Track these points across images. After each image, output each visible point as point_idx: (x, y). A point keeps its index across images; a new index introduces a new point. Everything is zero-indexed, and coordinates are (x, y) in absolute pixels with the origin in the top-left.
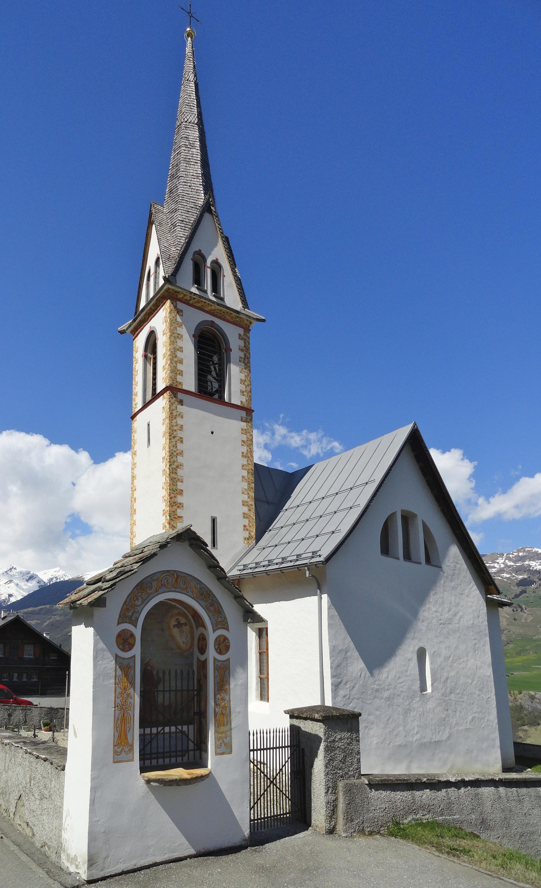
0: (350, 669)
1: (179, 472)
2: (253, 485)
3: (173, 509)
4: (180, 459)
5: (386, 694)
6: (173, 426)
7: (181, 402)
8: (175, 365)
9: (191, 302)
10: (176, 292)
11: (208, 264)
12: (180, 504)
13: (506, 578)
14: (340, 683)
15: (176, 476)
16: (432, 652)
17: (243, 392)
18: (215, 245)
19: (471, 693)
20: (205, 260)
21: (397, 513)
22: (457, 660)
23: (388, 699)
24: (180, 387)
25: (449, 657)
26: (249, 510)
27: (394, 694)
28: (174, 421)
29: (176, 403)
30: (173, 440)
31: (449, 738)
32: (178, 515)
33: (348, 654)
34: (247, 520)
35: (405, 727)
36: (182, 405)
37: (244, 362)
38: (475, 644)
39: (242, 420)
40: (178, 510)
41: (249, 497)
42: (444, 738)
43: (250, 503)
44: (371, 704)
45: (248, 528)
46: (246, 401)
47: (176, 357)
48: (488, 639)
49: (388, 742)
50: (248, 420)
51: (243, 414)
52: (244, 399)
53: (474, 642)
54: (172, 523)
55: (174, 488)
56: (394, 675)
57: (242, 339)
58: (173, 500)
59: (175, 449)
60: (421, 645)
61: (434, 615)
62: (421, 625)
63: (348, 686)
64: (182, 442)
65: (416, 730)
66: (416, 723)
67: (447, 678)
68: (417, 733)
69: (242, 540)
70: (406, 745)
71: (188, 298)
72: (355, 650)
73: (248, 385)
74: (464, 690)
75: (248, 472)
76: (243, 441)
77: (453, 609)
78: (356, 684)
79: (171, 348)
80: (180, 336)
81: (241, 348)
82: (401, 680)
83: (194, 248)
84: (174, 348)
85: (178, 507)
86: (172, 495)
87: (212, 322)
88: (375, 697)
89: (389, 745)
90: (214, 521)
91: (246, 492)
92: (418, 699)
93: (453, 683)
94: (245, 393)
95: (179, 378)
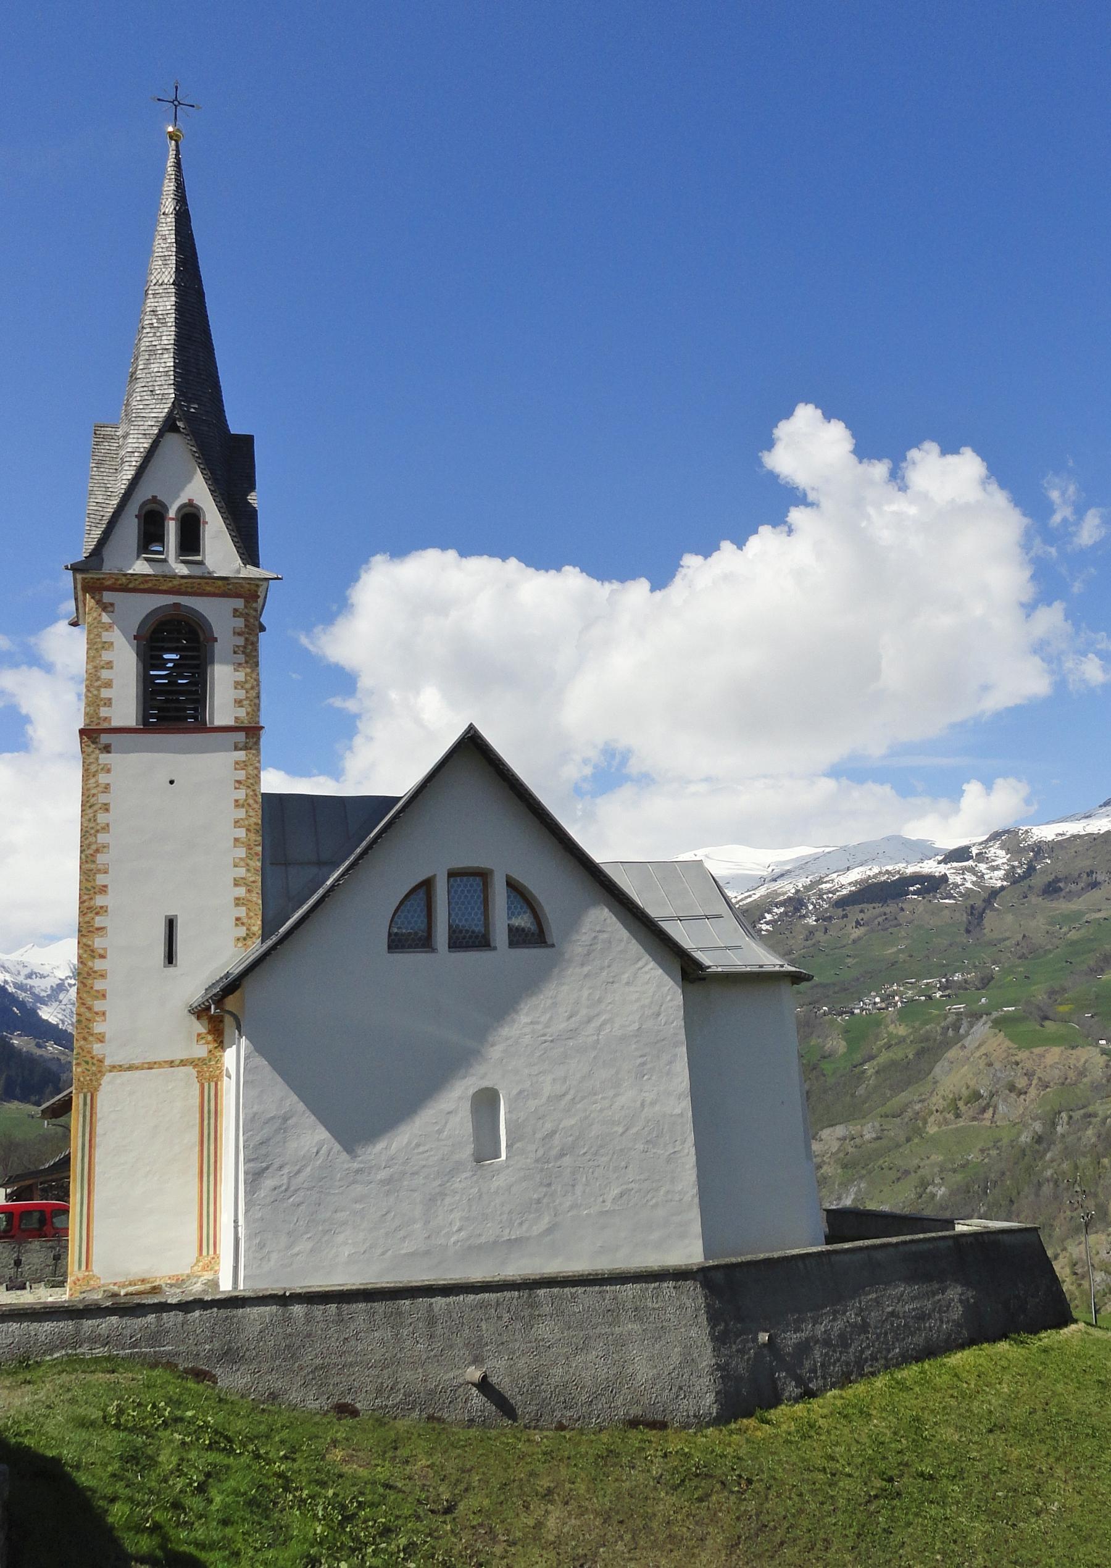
0: (292, 1145)
1: (101, 858)
2: (260, 849)
3: (87, 919)
4: (102, 838)
5: (382, 1175)
6: (88, 790)
7: (107, 749)
8: (95, 692)
9: (131, 586)
10: (98, 579)
11: (172, 513)
12: (101, 907)
13: (766, 930)
14: (267, 1168)
15: (93, 866)
16: (514, 1092)
17: (241, 701)
18: (189, 479)
19: (622, 1150)
20: (166, 509)
21: (438, 879)
22: (583, 1098)
23: (389, 1181)
24: (105, 725)
25: (564, 1095)
26: (249, 891)
27: (404, 1173)
28: (92, 781)
29: (97, 751)
30: (91, 811)
31: (549, 1231)
32: (97, 925)
33: (289, 1122)
34: (244, 908)
35: (427, 1223)
36: (109, 752)
37: (244, 653)
38: (643, 1064)
39: (236, 749)
40: (97, 918)
41: (248, 870)
42: (535, 1233)
43: (252, 879)
44: (342, 1193)
45: (245, 921)
46: (248, 714)
47: (98, 679)
48: (683, 1050)
49: (380, 1251)
50: (250, 744)
51: (241, 737)
52: (242, 713)
53: (639, 1061)
54: (84, 940)
55: (89, 885)
56: (405, 1141)
57: (241, 615)
58: (86, 904)
59: (91, 825)
60: (486, 1083)
61: (527, 1030)
62: (495, 1052)
63: (285, 1171)
64: (107, 810)
65: (458, 1224)
66: (457, 1215)
67: (553, 1133)
68: (460, 1230)
69: (233, 943)
70: (427, 1253)
71: (124, 580)
72: (308, 1113)
73: (252, 688)
74: (601, 1147)
75: (248, 830)
76: (239, 782)
77: (584, 1012)
78: (305, 1166)
79: (90, 667)
80: (108, 646)
81: (237, 630)
82: (421, 1149)
83: (143, 494)
84: (95, 667)
85: (97, 914)
86: (85, 897)
87: (176, 605)
88: (354, 1182)
89: (383, 1254)
90: (171, 924)
91: (242, 864)
92: (468, 1174)
93: (570, 1139)
94: (245, 702)
95: (104, 712)
